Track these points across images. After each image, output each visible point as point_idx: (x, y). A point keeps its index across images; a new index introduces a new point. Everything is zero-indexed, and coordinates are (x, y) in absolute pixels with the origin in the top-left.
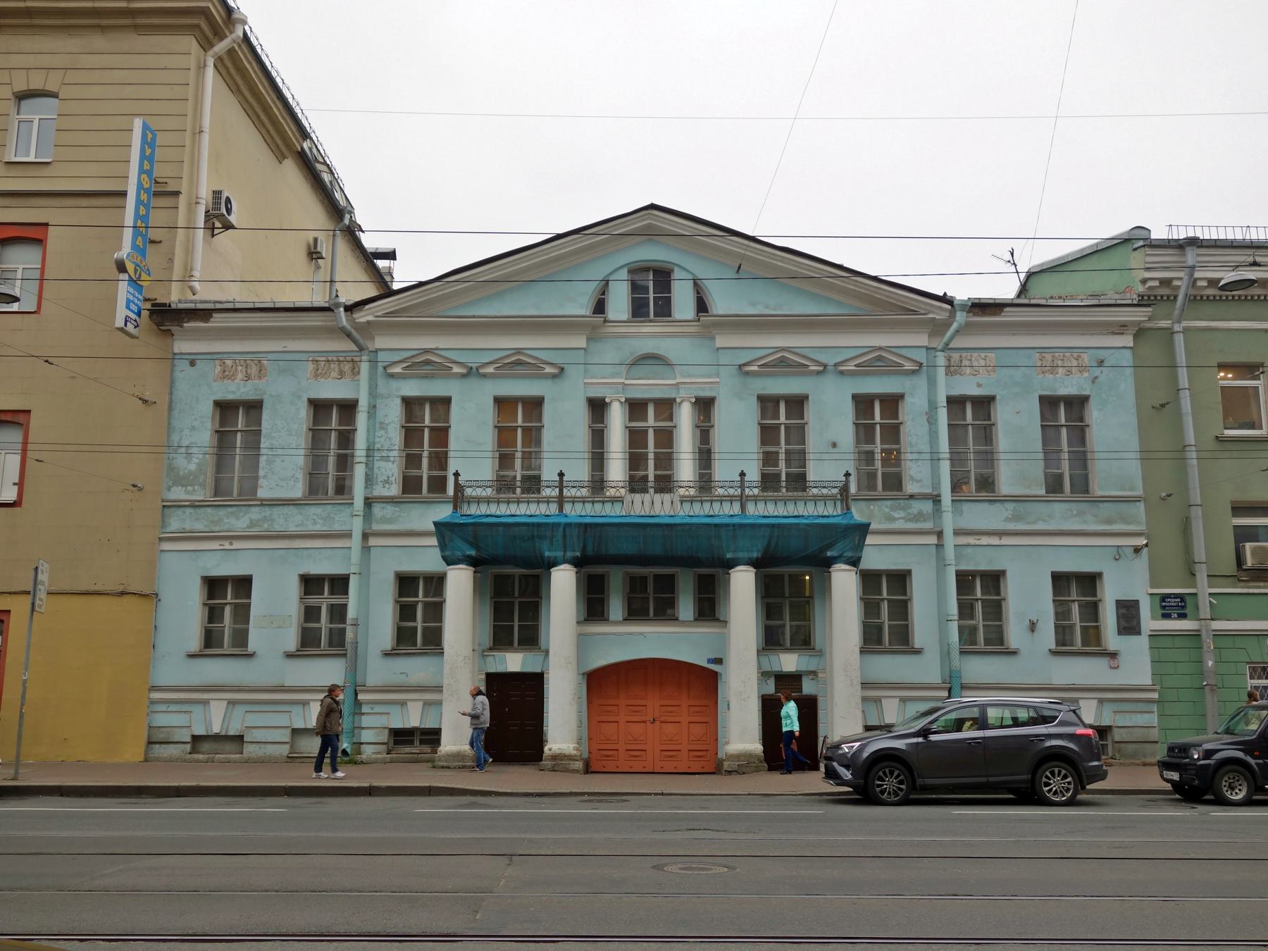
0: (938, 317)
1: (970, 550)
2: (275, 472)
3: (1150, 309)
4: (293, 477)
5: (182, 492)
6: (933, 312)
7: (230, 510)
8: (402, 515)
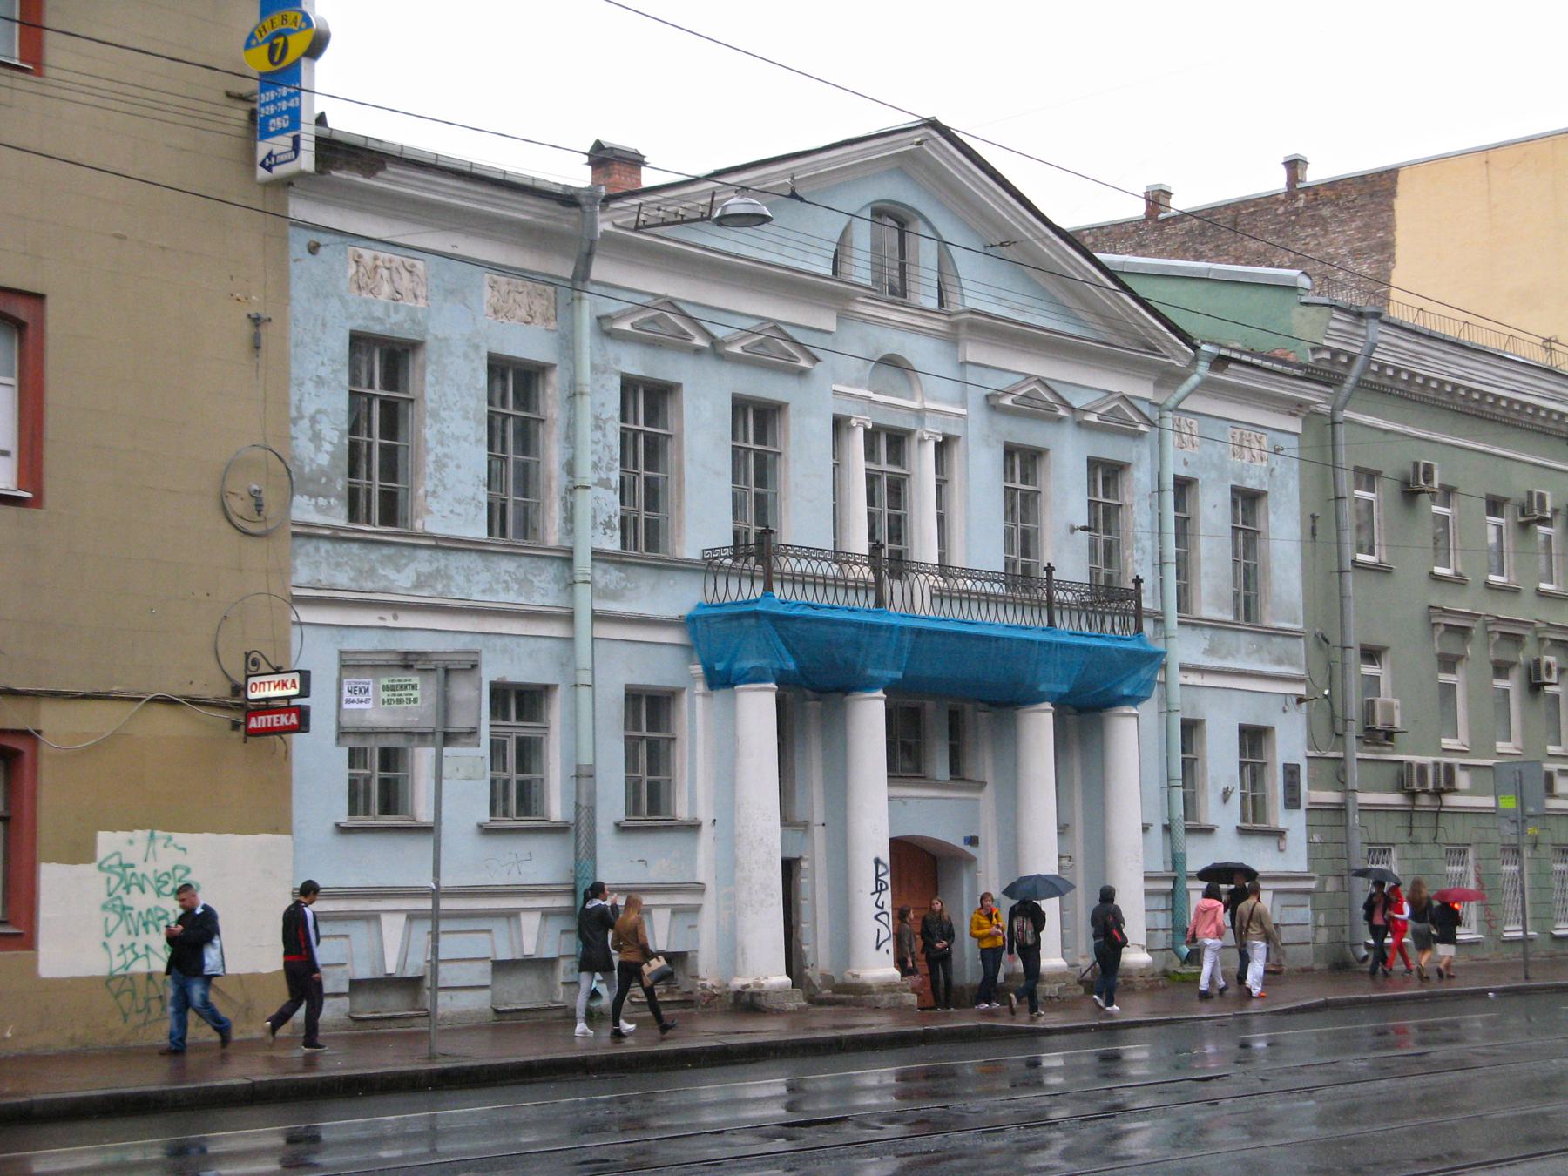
0: (1178, 364)
2: (449, 486)
3: (1331, 391)
4: (474, 499)
5: (311, 508)
6: (1174, 356)
7: (386, 551)
8: (629, 586)
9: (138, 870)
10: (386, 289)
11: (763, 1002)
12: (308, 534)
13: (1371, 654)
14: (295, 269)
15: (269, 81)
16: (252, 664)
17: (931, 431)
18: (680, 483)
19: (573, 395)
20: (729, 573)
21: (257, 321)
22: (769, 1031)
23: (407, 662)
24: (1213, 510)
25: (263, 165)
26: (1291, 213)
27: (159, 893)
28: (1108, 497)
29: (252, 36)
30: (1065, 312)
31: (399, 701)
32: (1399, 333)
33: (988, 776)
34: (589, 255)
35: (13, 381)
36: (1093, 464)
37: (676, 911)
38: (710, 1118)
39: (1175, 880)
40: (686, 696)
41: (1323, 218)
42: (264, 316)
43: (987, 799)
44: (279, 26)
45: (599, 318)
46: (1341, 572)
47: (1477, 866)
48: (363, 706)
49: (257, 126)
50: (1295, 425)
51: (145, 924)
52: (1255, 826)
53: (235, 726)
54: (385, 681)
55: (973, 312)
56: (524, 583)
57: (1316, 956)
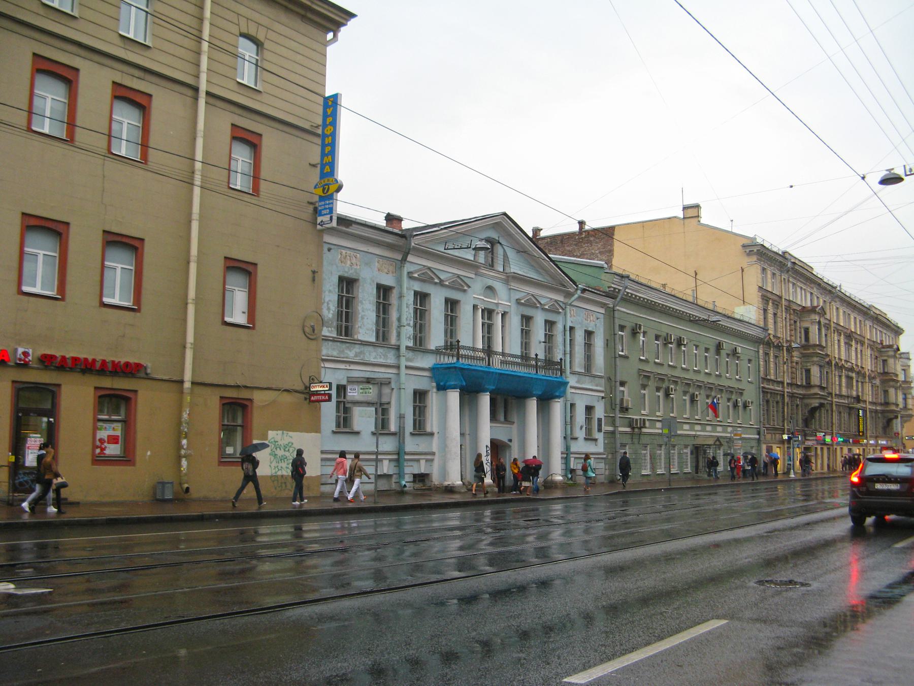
1: (671, 405)
7: (347, 345)
9: (279, 443)
10: (349, 262)
11: (455, 489)
12: (326, 339)
13: (622, 384)
14: (325, 256)
15: (321, 198)
16: (312, 380)
17: (501, 310)
18: (429, 326)
19: (401, 297)
20: (444, 354)
21: (314, 272)
22: (457, 498)
23: (368, 381)
24: (579, 337)
25: (319, 224)
26: (580, 239)
27: (285, 450)
28: (349, 294)
29: (317, 185)
30: (537, 272)
31: (366, 393)
32: (633, 283)
33: (516, 421)
34: (408, 253)
35: (247, 290)
36: (546, 321)
37: (427, 460)
38: (435, 525)
39: (567, 454)
40: (430, 393)
41: (591, 241)
42: (316, 271)
43: (514, 427)
44: (326, 182)
45: (408, 273)
46: (615, 358)
47: (650, 451)
48: (354, 394)
49: (316, 212)
50: (602, 311)
51: (281, 460)
52: (589, 438)
53: (306, 399)
54: (361, 387)
55: (514, 273)
56: (386, 357)
57: (605, 479)
